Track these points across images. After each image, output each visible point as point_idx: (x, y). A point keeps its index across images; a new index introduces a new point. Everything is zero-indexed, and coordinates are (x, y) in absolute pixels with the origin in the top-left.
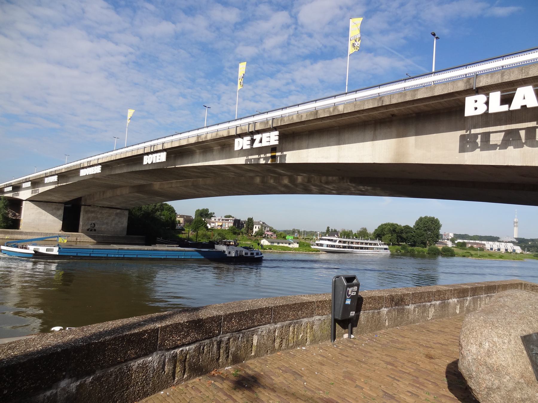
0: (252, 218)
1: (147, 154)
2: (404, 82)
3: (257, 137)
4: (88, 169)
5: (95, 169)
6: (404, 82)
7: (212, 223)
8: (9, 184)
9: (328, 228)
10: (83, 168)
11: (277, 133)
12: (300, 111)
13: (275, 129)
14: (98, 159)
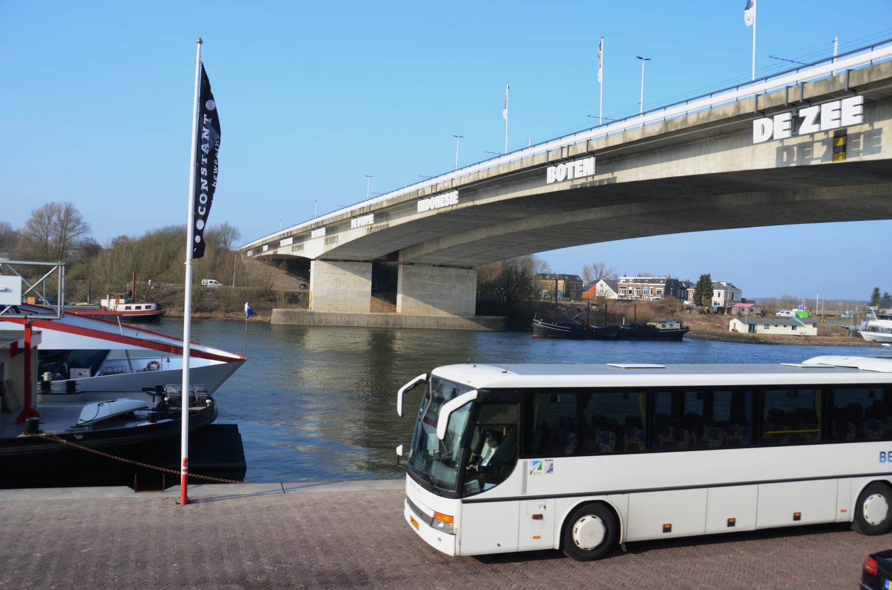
0: (709, 276)
1: (555, 163)
2: (870, 50)
3: (808, 113)
4: (432, 198)
5: (447, 199)
6: (870, 50)
7: (621, 288)
8: (288, 233)
9: (877, 290)
10: (422, 198)
11: (859, 99)
12: (666, 117)
13: (853, 91)
14: (452, 179)
